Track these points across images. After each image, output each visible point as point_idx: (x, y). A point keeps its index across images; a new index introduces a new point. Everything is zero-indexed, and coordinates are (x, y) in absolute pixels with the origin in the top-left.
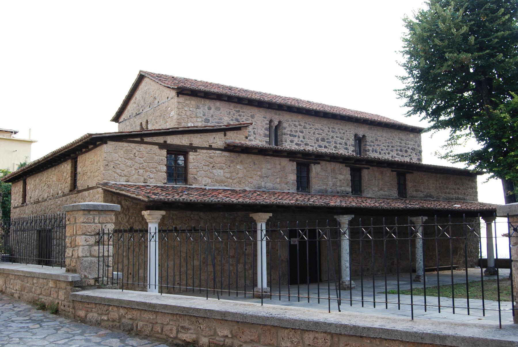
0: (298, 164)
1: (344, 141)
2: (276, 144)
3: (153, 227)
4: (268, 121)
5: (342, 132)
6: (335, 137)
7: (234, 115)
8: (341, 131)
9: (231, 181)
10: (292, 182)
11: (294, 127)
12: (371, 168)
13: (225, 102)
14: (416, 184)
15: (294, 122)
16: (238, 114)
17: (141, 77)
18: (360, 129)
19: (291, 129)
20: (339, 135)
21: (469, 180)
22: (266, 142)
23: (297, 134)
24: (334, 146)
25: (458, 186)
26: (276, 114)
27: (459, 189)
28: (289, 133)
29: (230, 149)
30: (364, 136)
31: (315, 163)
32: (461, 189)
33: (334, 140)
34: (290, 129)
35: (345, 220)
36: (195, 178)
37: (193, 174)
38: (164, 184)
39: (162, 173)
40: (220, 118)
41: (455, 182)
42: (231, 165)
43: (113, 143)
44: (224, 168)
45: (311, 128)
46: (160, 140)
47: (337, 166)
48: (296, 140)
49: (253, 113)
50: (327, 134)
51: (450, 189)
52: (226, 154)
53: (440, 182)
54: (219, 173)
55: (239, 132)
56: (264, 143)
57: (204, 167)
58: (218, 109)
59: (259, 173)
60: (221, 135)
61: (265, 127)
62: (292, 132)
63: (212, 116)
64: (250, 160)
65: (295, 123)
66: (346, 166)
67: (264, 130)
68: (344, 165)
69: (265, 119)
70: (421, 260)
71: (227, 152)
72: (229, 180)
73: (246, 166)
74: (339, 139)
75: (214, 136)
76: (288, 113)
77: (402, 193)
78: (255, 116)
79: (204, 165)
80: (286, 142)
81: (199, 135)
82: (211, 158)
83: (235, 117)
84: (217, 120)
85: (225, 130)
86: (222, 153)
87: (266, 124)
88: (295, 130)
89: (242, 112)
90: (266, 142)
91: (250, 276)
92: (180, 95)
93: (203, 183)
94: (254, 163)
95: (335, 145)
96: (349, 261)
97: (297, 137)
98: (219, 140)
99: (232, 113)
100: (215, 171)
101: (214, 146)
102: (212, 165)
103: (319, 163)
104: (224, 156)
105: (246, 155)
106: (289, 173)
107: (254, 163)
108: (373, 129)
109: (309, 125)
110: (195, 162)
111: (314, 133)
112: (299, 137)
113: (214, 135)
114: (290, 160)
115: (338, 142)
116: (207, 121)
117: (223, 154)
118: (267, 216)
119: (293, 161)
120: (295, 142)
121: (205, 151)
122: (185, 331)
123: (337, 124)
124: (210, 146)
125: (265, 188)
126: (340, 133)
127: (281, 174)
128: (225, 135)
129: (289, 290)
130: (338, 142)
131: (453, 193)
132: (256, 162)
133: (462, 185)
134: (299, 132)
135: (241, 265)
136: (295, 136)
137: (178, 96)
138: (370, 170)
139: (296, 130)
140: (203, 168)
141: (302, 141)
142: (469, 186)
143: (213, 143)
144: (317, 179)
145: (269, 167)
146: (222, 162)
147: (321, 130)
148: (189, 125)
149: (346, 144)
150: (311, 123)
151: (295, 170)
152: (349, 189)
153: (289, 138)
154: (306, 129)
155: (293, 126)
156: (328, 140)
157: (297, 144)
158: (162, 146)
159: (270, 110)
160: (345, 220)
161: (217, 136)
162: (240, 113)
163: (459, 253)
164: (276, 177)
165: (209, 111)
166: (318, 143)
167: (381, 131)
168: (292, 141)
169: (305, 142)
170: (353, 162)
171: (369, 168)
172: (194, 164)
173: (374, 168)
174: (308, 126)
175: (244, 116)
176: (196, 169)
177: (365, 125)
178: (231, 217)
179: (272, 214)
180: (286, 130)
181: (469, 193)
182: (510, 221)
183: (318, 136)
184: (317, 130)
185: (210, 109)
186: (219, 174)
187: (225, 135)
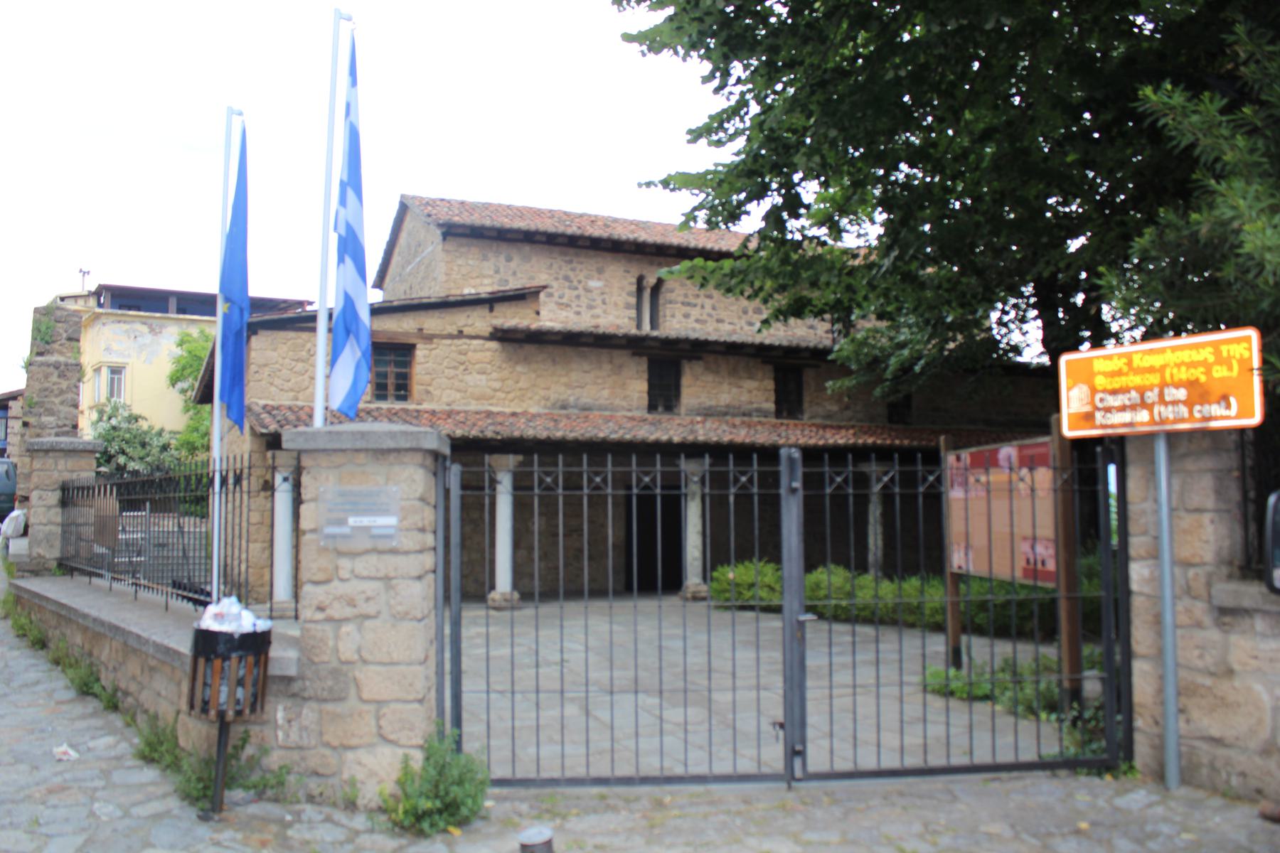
2: (654, 324)
9: (503, 395)
13: (541, 246)
17: (404, 208)
22: (630, 318)
23: (699, 301)
29: (503, 336)
31: (690, 359)
35: (692, 470)
36: (428, 392)
43: (269, 333)
44: (489, 371)
47: (621, 357)
48: (695, 313)
52: (494, 345)
54: (477, 381)
56: (626, 320)
57: (446, 371)
80: (673, 316)
81: (436, 313)
82: (460, 353)
85: (491, 302)
90: (630, 318)
98: (480, 321)
100: (468, 378)
101: (467, 331)
102: (462, 368)
103: (699, 358)
104: (488, 350)
105: (537, 346)
112: (703, 307)
118: (512, 460)
120: (693, 318)
121: (448, 342)
122: (99, 671)
129: (660, 620)
136: (695, 305)
137: (444, 239)
140: (443, 372)
141: (710, 315)
148: (466, 291)
152: (771, 406)
153: (679, 310)
157: (697, 321)
168: (687, 316)
172: (427, 365)
187: (491, 310)
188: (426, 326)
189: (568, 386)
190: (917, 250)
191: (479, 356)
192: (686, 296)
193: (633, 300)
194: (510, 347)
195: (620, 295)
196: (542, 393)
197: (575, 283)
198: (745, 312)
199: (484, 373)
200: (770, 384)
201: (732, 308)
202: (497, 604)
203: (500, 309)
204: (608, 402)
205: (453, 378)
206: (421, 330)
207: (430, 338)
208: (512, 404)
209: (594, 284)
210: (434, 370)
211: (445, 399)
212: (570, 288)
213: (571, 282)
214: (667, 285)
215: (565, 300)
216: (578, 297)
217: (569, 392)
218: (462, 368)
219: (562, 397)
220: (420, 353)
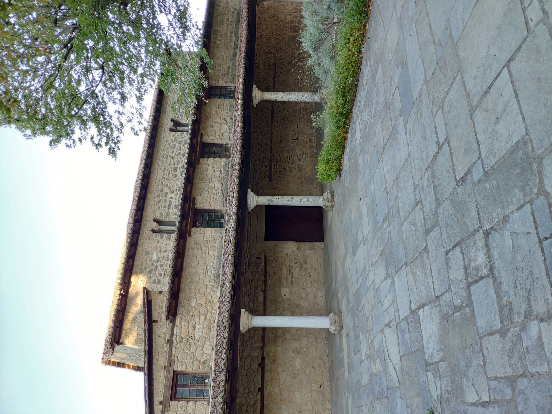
0: (194, 226)
1: (177, 145)
2: (172, 224)
3: (264, 200)
4: (152, 235)
5: (168, 146)
6: (173, 155)
8: (166, 148)
9: (209, 314)
10: (213, 234)
12: (201, 131)
14: (220, 74)
16: (143, 270)
17: (109, 363)
18: (164, 124)
19: (162, 207)
20: (170, 150)
21: (219, 6)
23: (168, 200)
24: (182, 157)
25: (225, 20)
26: (146, 225)
27: (228, 20)
28: (166, 210)
30: (172, 120)
31: (194, 204)
32: (227, 17)
33: (176, 156)
35: (257, 95)
36: (204, 363)
37: (199, 366)
38: (209, 405)
41: (220, 24)
42: (191, 313)
45: (162, 184)
47: (191, 242)
49: (144, 253)
50: (170, 164)
51: (227, 30)
52: (178, 320)
53: (219, 43)
55: (154, 303)
60: (155, 326)
61: (159, 238)
64: (187, 288)
65: (156, 203)
66: (198, 164)
67: (163, 240)
69: (151, 239)
70: (303, 96)
71: (176, 319)
72: (208, 317)
73: (193, 293)
74: (175, 151)
75: (157, 336)
76: (145, 210)
77: (229, 94)
78: (146, 250)
79: (189, 351)
81: (155, 357)
82: (181, 341)
86: (177, 326)
87: (156, 237)
88: (163, 202)
92: (121, 341)
93: (210, 351)
94: (190, 283)
95: (181, 156)
96: (301, 197)
97: (172, 200)
100: (197, 336)
102: (190, 340)
103: (194, 198)
104: (180, 323)
105: (180, 293)
107: (190, 283)
108: (164, 109)
110: (185, 363)
111: (168, 180)
112: (172, 198)
113: (155, 336)
114: (190, 235)
115: (178, 151)
116: (168, 258)
117: (178, 325)
118: (244, 314)
119: (190, 231)
121: (174, 349)
123: (158, 152)
126: (168, 149)
127: (204, 247)
128: (156, 322)
130: (178, 151)
131: (231, 27)
132: (190, 280)
133: (223, 15)
135: (301, 303)
136: (171, 202)
138: (204, 133)
142: (225, 6)
143: (165, 338)
144: (211, 202)
145: (196, 263)
146: (187, 326)
147: (164, 171)
149: (180, 142)
151: (200, 229)
152: (223, 161)
154: (163, 189)
156: (176, 163)
159: (141, 232)
160: (257, 95)
161: (158, 332)
162: (143, 268)
163: (297, 24)
164: (207, 254)
166: (182, 160)
167: (166, 99)
169: (177, 191)
170: (194, 154)
171: (202, 134)
172: (187, 363)
173: (201, 128)
174: (160, 187)
175: (147, 264)
176: (193, 362)
177: (161, 118)
179: (242, 310)
180: (164, 213)
181: (232, 7)
183: (171, 175)
184: (165, 176)
186: (200, 329)
187: (156, 322)
188: (163, 365)
189: (206, 274)
190: (125, 60)
191: (184, 330)
192: (165, 207)
193: (166, 235)
194: (180, 310)
195: (162, 242)
196: (209, 290)
197: (154, 267)
198: (176, 176)
200: (211, 160)
201: (173, 183)
202: (338, 329)
204: (216, 250)
205: (196, 346)
207: (171, 362)
208: (214, 308)
209: (154, 257)
213: (152, 269)
214: (158, 217)
215: (163, 273)
216: (161, 266)
217: (209, 274)
218: (190, 340)
219: (212, 278)
220: (179, 368)
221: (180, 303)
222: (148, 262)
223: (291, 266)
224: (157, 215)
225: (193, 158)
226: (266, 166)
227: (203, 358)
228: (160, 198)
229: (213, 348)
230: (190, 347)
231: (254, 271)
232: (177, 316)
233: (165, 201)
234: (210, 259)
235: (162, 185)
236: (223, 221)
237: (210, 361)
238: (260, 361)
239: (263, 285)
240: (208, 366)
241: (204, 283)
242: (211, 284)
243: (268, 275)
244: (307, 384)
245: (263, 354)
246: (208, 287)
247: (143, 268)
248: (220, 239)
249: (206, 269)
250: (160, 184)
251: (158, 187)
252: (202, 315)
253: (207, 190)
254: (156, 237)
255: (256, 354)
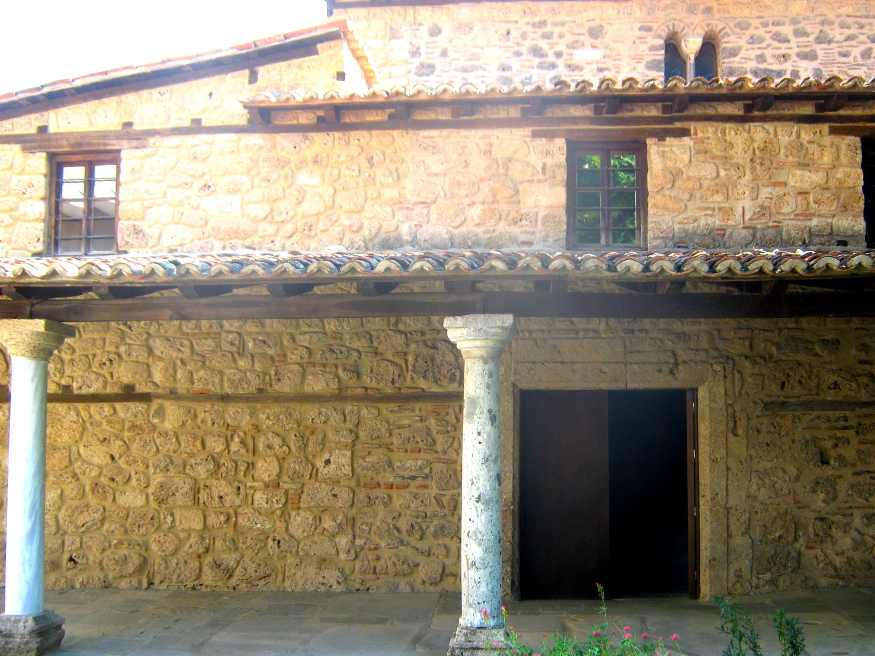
4: (659, 36)
7: (524, 36)
9: (272, 229)
11: (776, 44)
15: (770, 28)
19: (759, 52)
31: (661, 135)
34: (753, 54)
36: (137, 231)
37: (129, 219)
39: (29, 225)
40: (473, 55)
45: (849, 38)
46: (26, 125)
52: (256, 139)
58: (466, 28)
59: (389, 194)
61: (649, 58)
62: (764, 61)
63: (444, 54)
68: (825, 127)
69: (644, 34)
72: (263, 226)
75: (210, 89)
83: (528, 43)
84: (459, 64)
89: (556, 24)
91: (343, 556)
99: (515, 33)
103: (685, 133)
106: (532, 181)
109: (843, 26)
114: (536, 135)
116: (427, 69)
124: (193, 121)
125: (414, 242)
128: (253, 79)
134: (794, 58)
135: (302, 513)
139: (783, 52)
145: (436, 168)
150: (850, 21)
154: (830, 42)
155: (769, 41)
158: (28, 143)
162: (549, 28)
165: (434, 39)
175: (561, 36)
178: (271, 352)
180: (737, 59)
182: (28, 312)
185: (435, 32)
199: (236, 191)
203: (268, 73)
206: (128, 125)
210: (810, 220)
211: (166, 242)
212: (541, 66)
221: (307, 138)
222: (569, 38)
223: (428, 482)
224: (732, 38)
225: (638, 112)
226: (836, 386)
227: (150, 227)
228: (794, 40)
229: (176, 250)
230: (178, 186)
231: (406, 361)
232: (267, 136)
233: (785, 57)
234: (451, 213)
235: (841, 38)
236: (603, 241)
237: (140, 245)
238: (140, 389)
239: (359, 391)
240: (127, 243)
241: (369, 203)
242: (366, 223)
243: (394, 406)
244: (79, 523)
245: (159, 396)
246: (357, 216)
247: (549, 28)
248: (523, 237)
249: (416, 204)
250: (847, 32)
251: (836, 25)
252: (268, 210)
253: (722, 173)
254: (653, 48)
255: (158, 377)
